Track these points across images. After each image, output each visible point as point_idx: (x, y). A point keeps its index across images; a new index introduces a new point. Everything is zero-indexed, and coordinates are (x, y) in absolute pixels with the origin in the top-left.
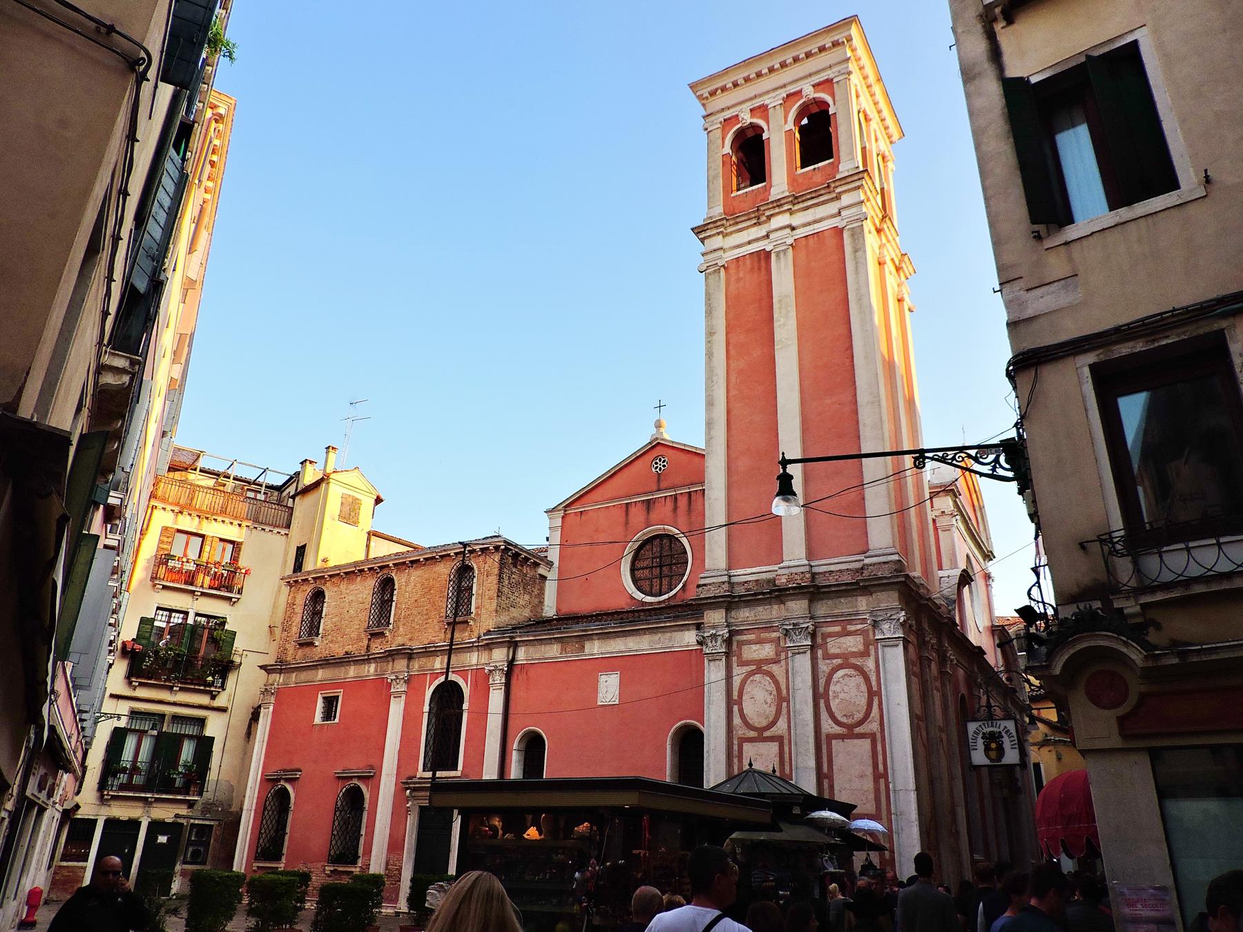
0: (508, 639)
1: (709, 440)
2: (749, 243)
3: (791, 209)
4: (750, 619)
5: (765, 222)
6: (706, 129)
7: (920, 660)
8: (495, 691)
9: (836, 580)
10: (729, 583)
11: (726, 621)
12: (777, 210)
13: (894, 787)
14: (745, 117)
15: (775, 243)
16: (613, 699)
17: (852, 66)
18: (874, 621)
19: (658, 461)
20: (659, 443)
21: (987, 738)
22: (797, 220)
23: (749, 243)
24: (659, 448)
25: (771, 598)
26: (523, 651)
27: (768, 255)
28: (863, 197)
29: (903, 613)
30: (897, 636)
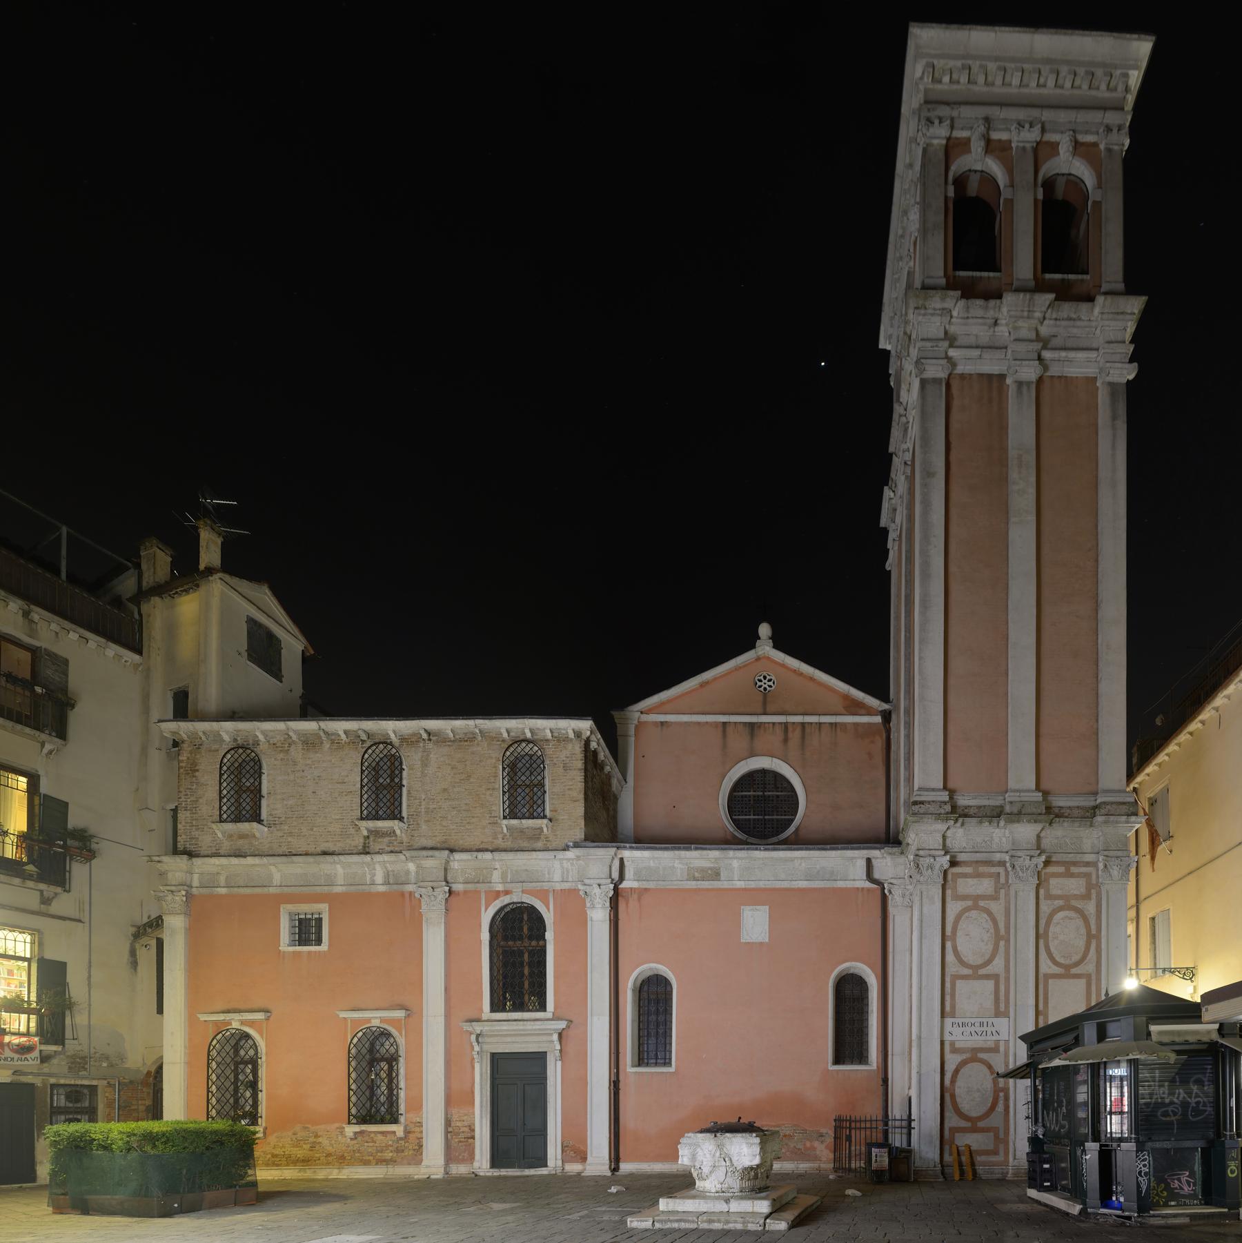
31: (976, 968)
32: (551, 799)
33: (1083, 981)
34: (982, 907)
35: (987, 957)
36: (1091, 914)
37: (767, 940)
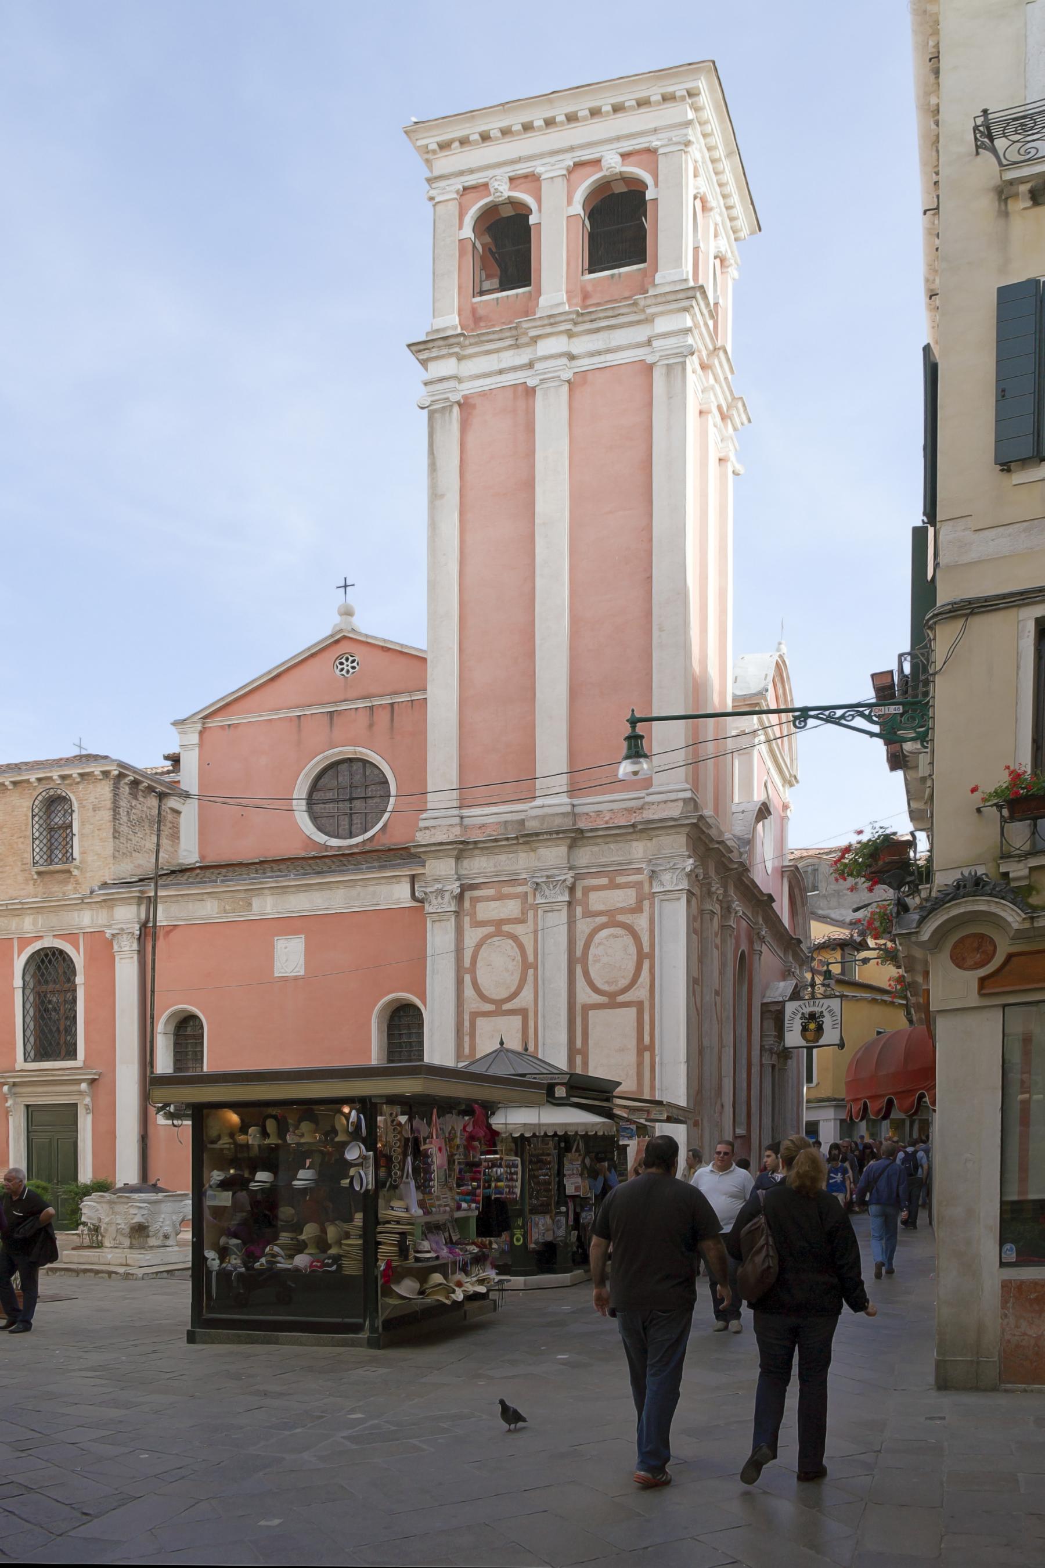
1: (434, 638)
2: (501, 372)
3: (571, 330)
5: (527, 345)
6: (431, 199)
7: (702, 914)
8: (123, 961)
9: (607, 823)
10: (461, 824)
11: (456, 873)
12: (549, 330)
13: (661, 1058)
14: (501, 188)
15: (542, 377)
16: (297, 969)
17: (693, 133)
18: (653, 871)
19: (343, 660)
20: (345, 637)
21: (806, 1018)
22: (579, 346)
23: (501, 372)
24: (343, 643)
25: (518, 844)
27: (530, 392)
28: (689, 323)
29: (691, 861)
31: (499, 1002)
32: (80, 841)
33: (633, 1011)
35: (513, 989)
37: (302, 973)
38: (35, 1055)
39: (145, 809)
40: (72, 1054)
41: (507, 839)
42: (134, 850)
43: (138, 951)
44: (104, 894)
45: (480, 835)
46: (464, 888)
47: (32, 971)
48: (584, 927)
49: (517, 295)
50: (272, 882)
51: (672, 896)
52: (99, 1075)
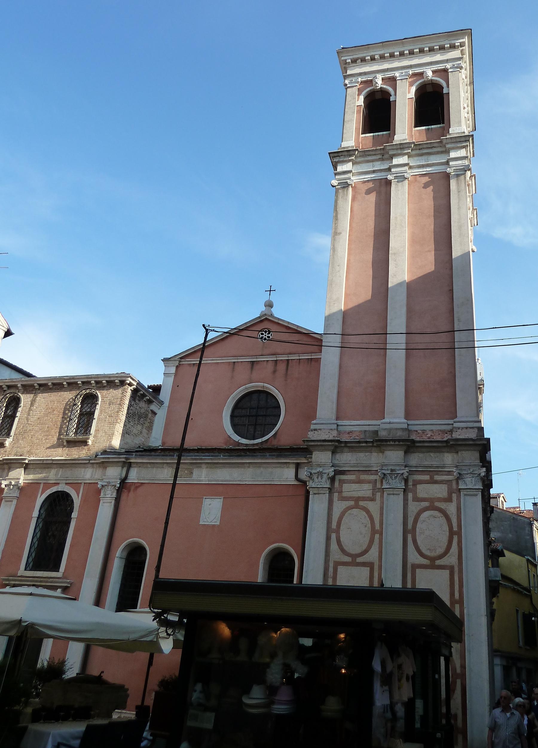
0: (124, 460)
4: (352, 462)
5: (387, 159)
8: (105, 504)
9: (429, 438)
12: (399, 152)
18: (460, 474)
20: (266, 319)
25: (373, 446)
26: (135, 471)
30: (477, 488)
31: (354, 556)
34: (362, 506)
35: (364, 548)
36: (453, 513)
37: (218, 523)
38: (33, 566)
39: (138, 408)
40: (56, 568)
41: (366, 442)
42: (126, 433)
43: (115, 498)
44: (103, 458)
45: (348, 438)
46: (338, 472)
47: (46, 506)
48: (414, 507)
49: (383, 135)
50: (209, 459)
51: (471, 493)
52: (71, 584)
